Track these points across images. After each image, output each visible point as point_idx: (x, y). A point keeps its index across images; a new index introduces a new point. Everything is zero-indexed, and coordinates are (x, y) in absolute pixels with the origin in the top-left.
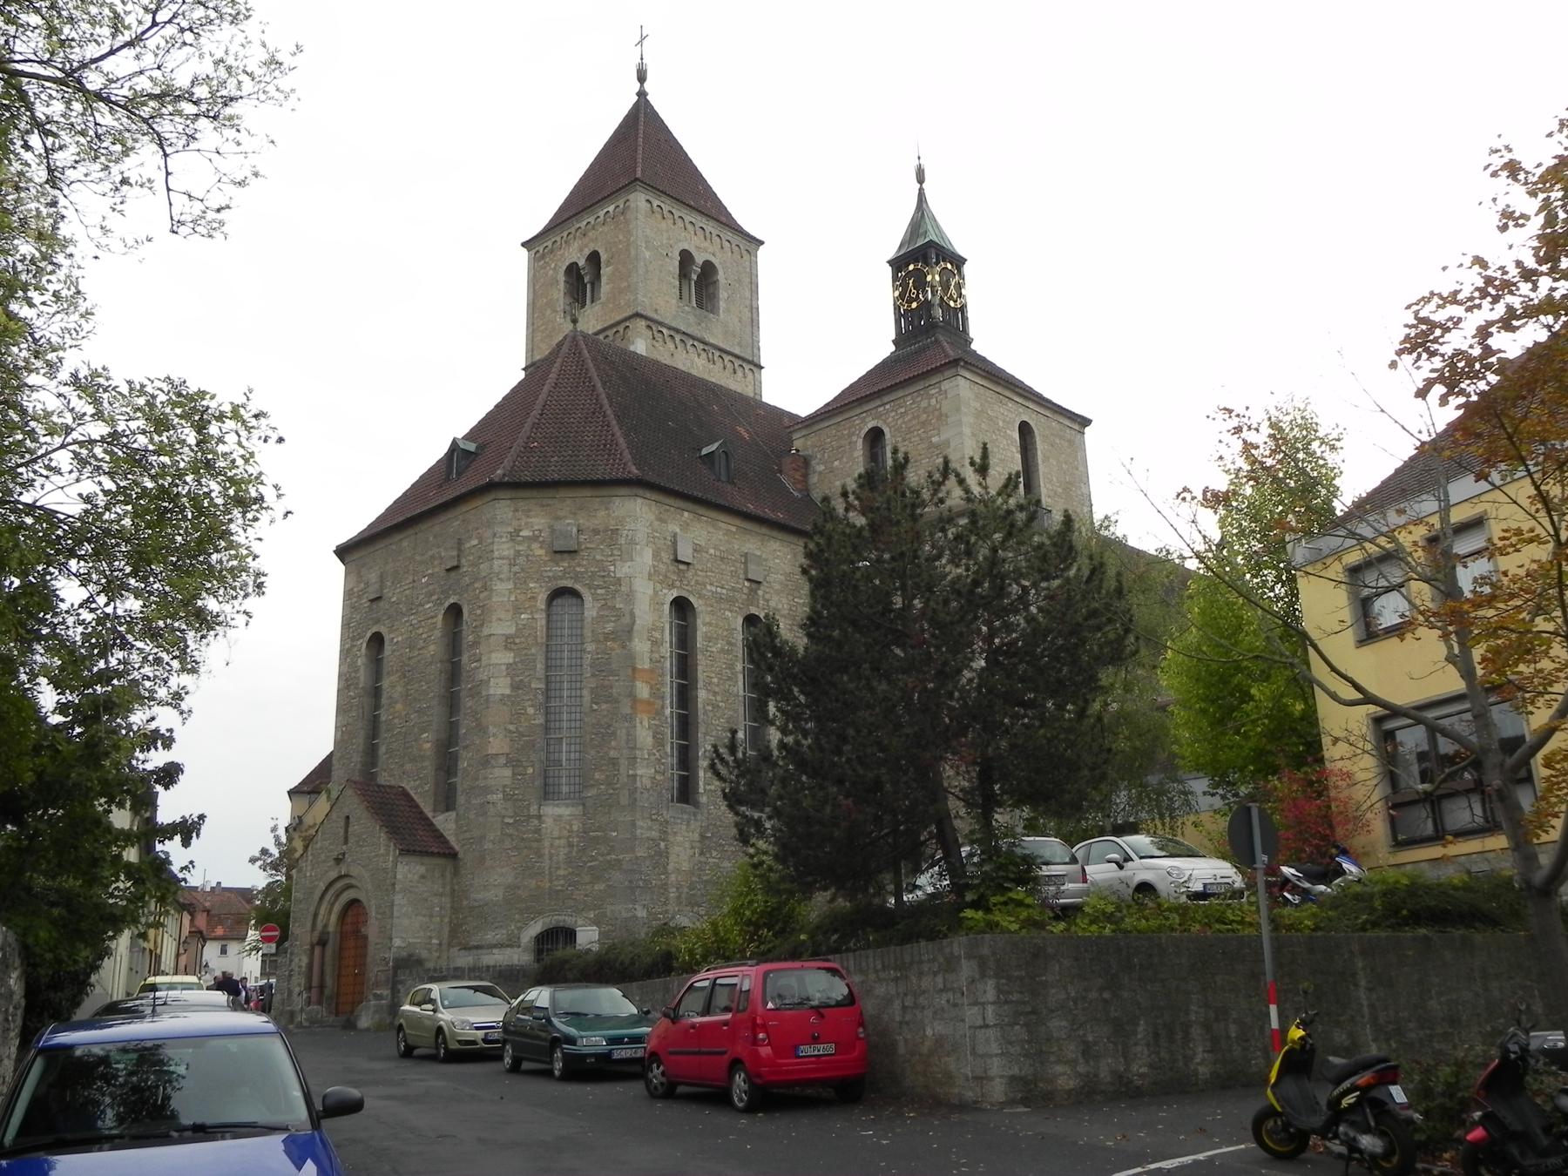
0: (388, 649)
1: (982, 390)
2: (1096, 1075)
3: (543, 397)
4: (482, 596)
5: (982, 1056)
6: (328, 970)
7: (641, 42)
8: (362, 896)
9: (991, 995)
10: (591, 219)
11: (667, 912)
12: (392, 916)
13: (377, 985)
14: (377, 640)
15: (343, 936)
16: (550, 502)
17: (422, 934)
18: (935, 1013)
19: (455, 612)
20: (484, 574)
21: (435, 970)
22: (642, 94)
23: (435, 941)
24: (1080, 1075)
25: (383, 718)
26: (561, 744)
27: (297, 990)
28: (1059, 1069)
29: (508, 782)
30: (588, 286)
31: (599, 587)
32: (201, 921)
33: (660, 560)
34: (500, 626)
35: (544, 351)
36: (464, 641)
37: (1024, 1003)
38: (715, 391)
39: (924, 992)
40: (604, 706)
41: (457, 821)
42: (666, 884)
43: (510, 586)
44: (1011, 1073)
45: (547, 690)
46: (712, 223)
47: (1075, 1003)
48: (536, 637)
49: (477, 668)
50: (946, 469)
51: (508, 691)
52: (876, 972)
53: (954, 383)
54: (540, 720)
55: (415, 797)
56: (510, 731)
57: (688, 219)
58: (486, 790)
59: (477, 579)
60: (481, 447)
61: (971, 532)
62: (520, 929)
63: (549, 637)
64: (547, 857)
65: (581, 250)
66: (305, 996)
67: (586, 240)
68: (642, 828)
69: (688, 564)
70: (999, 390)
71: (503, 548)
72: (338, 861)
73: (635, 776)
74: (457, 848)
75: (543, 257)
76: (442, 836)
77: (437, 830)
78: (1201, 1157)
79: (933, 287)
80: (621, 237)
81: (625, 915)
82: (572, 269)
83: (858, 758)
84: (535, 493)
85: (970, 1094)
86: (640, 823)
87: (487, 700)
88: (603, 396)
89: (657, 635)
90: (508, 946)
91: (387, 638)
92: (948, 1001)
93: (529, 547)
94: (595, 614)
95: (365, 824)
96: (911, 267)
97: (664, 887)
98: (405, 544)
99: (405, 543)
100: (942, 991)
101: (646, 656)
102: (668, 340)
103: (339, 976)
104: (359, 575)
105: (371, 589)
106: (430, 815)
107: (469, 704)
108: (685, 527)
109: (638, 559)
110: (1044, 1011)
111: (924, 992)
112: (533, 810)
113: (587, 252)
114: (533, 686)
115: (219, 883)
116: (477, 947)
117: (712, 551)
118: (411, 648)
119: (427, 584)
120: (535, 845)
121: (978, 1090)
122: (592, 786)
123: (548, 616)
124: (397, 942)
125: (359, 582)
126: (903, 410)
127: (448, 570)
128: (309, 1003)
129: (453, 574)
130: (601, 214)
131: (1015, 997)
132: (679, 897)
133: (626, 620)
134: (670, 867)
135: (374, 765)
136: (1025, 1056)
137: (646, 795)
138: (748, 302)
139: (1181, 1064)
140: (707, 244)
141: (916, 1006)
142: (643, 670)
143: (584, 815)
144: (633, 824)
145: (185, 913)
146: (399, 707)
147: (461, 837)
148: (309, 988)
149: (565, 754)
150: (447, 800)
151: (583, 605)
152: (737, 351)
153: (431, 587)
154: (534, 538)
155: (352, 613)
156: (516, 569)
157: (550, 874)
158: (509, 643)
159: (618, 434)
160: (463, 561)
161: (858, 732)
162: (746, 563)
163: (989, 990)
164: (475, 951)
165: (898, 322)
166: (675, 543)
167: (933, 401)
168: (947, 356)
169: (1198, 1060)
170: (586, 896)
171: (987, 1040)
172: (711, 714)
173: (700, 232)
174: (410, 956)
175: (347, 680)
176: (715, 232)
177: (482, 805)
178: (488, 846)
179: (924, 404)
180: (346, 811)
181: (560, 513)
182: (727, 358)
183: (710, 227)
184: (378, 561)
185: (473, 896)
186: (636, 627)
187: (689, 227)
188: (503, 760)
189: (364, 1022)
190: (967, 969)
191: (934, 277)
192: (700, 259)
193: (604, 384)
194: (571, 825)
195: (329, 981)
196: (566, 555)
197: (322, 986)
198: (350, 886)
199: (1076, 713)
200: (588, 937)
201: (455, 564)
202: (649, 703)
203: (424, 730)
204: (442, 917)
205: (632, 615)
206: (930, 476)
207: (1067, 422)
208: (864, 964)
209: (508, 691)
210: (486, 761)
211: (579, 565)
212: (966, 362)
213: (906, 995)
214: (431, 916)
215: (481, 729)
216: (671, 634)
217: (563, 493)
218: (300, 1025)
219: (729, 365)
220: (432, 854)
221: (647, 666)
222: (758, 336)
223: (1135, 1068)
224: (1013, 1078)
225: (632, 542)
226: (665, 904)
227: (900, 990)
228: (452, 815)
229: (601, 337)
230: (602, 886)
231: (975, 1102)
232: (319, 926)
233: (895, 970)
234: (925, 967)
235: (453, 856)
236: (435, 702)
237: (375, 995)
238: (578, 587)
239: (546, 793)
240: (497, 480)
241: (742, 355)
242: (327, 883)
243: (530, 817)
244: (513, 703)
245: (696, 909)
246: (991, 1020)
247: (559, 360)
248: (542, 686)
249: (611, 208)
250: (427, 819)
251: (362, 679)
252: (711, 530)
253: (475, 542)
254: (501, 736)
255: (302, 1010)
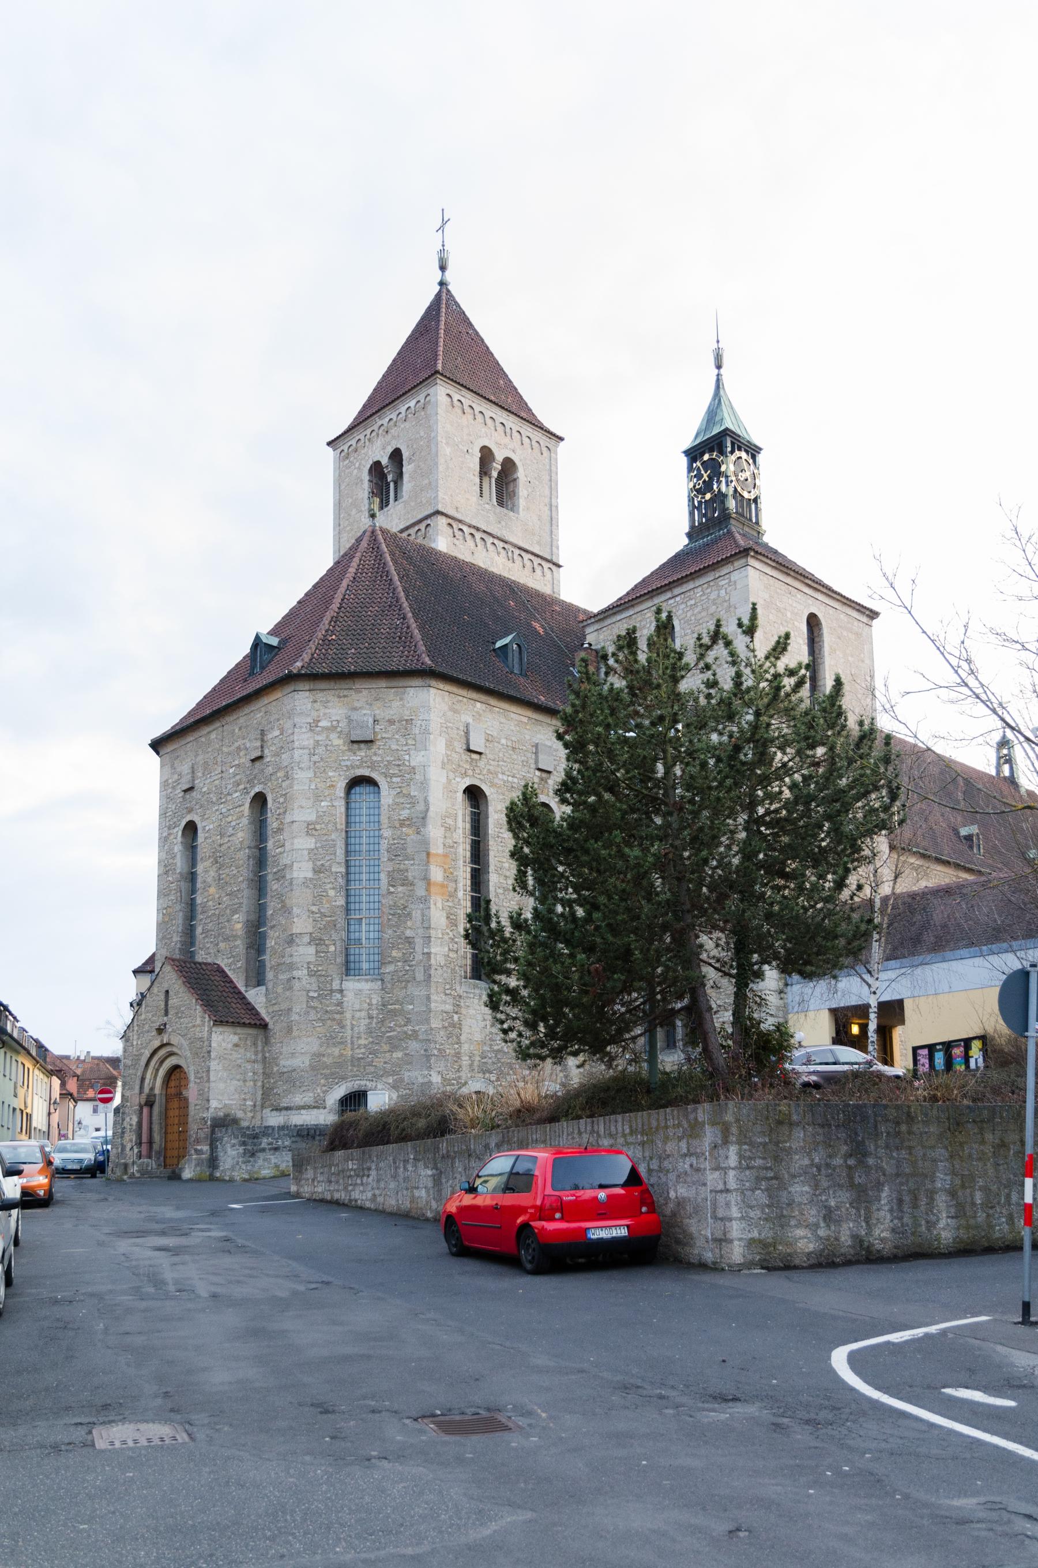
0: (201, 836)
1: (772, 580)
2: (837, 1239)
3: (342, 589)
4: (284, 784)
5: (722, 1219)
6: (156, 1128)
7: (442, 228)
8: (182, 1063)
9: (733, 1160)
10: (393, 416)
11: (460, 1078)
12: (208, 1081)
13: (198, 1141)
14: (191, 828)
15: (168, 1098)
16: (346, 693)
17: (237, 1096)
18: (679, 1176)
19: (260, 800)
20: (285, 764)
21: (248, 1128)
22: (442, 283)
23: (250, 1103)
24: (821, 1238)
25: (199, 901)
26: (360, 924)
27: (129, 1146)
28: (800, 1232)
29: (312, 959)
30: (392, 485)
31: (394, 775)
32: (72, 1086)
33: (453, 750)
34: (302, 813)
35: (347, 544)
36: (269, 828)
37: (767, 1169)
38: (512, 588)
39: (668, 1156)
40: (400, 889)
41: (266, 995)
42: (459, 1053)
43: (311, 774)
44: (750, 1236)
45: (348, 873)
46: (512, 418)
47: (819, 1170)
48: (336, 823)
49: (281, 853)
50: (716, 636)
51: (310, 875)
52: (624, 1135)
53: (744, 573)
54: (341, 901)
55: (229, 973)
56: (313, 912)
57: (488, 414)
58: (291, 967)
59: (279, 769)
60: (283, 642)
61: (735, 695)
62: (326, 1091)
63: (348, 823)
64: (349, 1027)
65: (384, 448)
66: (136, 1150)
67: (389, 437)
68: (436, 1001)
69: (480, 754)
70: (789, 580)
71: (303, 739)
72: (160, 1031)
73: (429, 954)
74: (267, 1019)
75: (347, 456)
76: (254, 1008)
77: (249, 1003)
78: (933, 1329)
79: (727, 477)
80: (422, 434)
81: (421, 1080)
82: (376, 469)
83: (609, 925)
84: (332, 684)
85: (710, 1255)
86: (433, 997)
87: (291, 884)
88: (400, 589)
89: (450, 821)
90: (315, 1107)
91: (199, 826)
92: (691, 1166)
93: (327, 737)
94: (391, 802)
95: (183, 998)
96: (706, 457)
97: (458, 1055)
98: (213, 736)
99: (212, 734)
100: (685, 1155)
101: (441, 841)
102: (469, 538)
103: (166, 1133)
104: (173, 767)
105: (183, 780)
106: (243, 989)
107: (275, 887)
108: (478, 717)
109: (432, 748)
110: (786, 1176)
111: (668, 1156)
112: (336, 985)
113: (390, 450)
114: (333, 870)
115: (88, 1053)
116: (287, 1109)
117: (503, 741)
118: (222, 835)
119: (236, 775)
120: (337, 1017)
121: (717, 1251)
122: (390, 962)
123: (347, 803)
124: (214, 1104)
125: (173, 774)
126: (692, 602)
127: (253, 761)
128: (140, 1157)
129: (257, 764)
130: (403, 409)
131: (759, 1162)
132: (471, 1065)
133: (421, 807)
134: (463, 1038)
135: (192, 944)
136: (766, 1219)
137: (440, 972)
138: (547, 500)
139: (923, 1228)
140: (507, 440)
141: (661, 1169)
142: (437, 855)
143: (383, 989)
144: (428, 998)
145: (54, 1078)
146: (212, 890)
147: (270, 1010)
148: (140, 1144)
149: (366, 933)
150: (258, 977)
151: (379, 793)
152: (536, 551)
153: (238, 777)
154: (333, 728)
155: (168, 803)
156: (316, 758)
157: (352, 1043)
158: (310, 829)
159: (414, 625)
160: (266, 751)
161: (610, 898)
162: (536, 753)
163: (732, 1155)
164: (284, 1112)
165: (691, 514)
166: (467, 733)
167: (723, 592)
168: (738, 546)
169: (942, 1226)
170: (385, 1063)
171: (728, 1205)
172: (501, 897)
173: (500, 428)
174: (227, 1116)
175: (165, 866)
176: (515, 428)
177: (289, 980)
178: (295, 1017)
179: (713, 596)
180: (166, 986)
181: (357, 704)
182: (526, 556)
183: (511, 422)
184: (188, 748)
185: (282, 1063)
186: (431, 814)
187: (489, 422)
188: (306, 939)
189: (187, 1174)
190: (710, 1135)
191: (728, 466)
192: (499, 456)
193: (401, 579)
194: (371, 999)
195: (157, 1137)
196: (362, 745)
197: (150, 1142)
198: (171, 1054)
199: (834, 881)
200: (379, 1100)
201: (259, 754)
202: (443, 886)
203: (235, 912)
204: (255, 1081)
205: (426, 801)
206: (699, 639)
207: (855, 614)
208: (613, 1128)
209: (310, 875)
210: (291, 941)
211: (375, 754)
212: (757, 552)
213: (651, 1158)
214: (245, 1081)
215: (286, 910)
216: (464, 821)
217: (359, 684)
218: (132, 1176)
219: (528, 564)
220: (244, 1025)
221: (440, 851)
222: (557, 535)
223: (877, 1232)
224: (751, 1242)
225: (427, 732)
226: (458, 1071)
227: (647, 1154)
228: (262, 989)
229: (404, 535)
230: (400, 1054)
231: (714, 1263)
232: (146, 1090)
233: (642, 1135)
234: (671, 1132)
235: (264, 1026)
236: (244, 886)
237: (196, 1150)
238: (374, 775)
239: (348, 970)
240: (295, 671)
241: (541, 554)
242: (151, 1051)
243: (332, 991)
244: (315, 886)
245: (487, 1075)
246: (732, 1184)
247: (358, 554)
248: (343, 870)
249: (412, 404)
250: (240, 993)
251: (179, 864)
252: (503, 720)
253: (277, 733)
254: (304, 917)
255: (133, 1163)
